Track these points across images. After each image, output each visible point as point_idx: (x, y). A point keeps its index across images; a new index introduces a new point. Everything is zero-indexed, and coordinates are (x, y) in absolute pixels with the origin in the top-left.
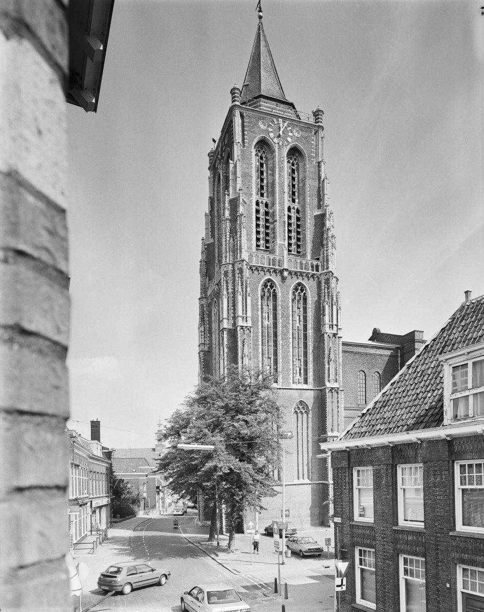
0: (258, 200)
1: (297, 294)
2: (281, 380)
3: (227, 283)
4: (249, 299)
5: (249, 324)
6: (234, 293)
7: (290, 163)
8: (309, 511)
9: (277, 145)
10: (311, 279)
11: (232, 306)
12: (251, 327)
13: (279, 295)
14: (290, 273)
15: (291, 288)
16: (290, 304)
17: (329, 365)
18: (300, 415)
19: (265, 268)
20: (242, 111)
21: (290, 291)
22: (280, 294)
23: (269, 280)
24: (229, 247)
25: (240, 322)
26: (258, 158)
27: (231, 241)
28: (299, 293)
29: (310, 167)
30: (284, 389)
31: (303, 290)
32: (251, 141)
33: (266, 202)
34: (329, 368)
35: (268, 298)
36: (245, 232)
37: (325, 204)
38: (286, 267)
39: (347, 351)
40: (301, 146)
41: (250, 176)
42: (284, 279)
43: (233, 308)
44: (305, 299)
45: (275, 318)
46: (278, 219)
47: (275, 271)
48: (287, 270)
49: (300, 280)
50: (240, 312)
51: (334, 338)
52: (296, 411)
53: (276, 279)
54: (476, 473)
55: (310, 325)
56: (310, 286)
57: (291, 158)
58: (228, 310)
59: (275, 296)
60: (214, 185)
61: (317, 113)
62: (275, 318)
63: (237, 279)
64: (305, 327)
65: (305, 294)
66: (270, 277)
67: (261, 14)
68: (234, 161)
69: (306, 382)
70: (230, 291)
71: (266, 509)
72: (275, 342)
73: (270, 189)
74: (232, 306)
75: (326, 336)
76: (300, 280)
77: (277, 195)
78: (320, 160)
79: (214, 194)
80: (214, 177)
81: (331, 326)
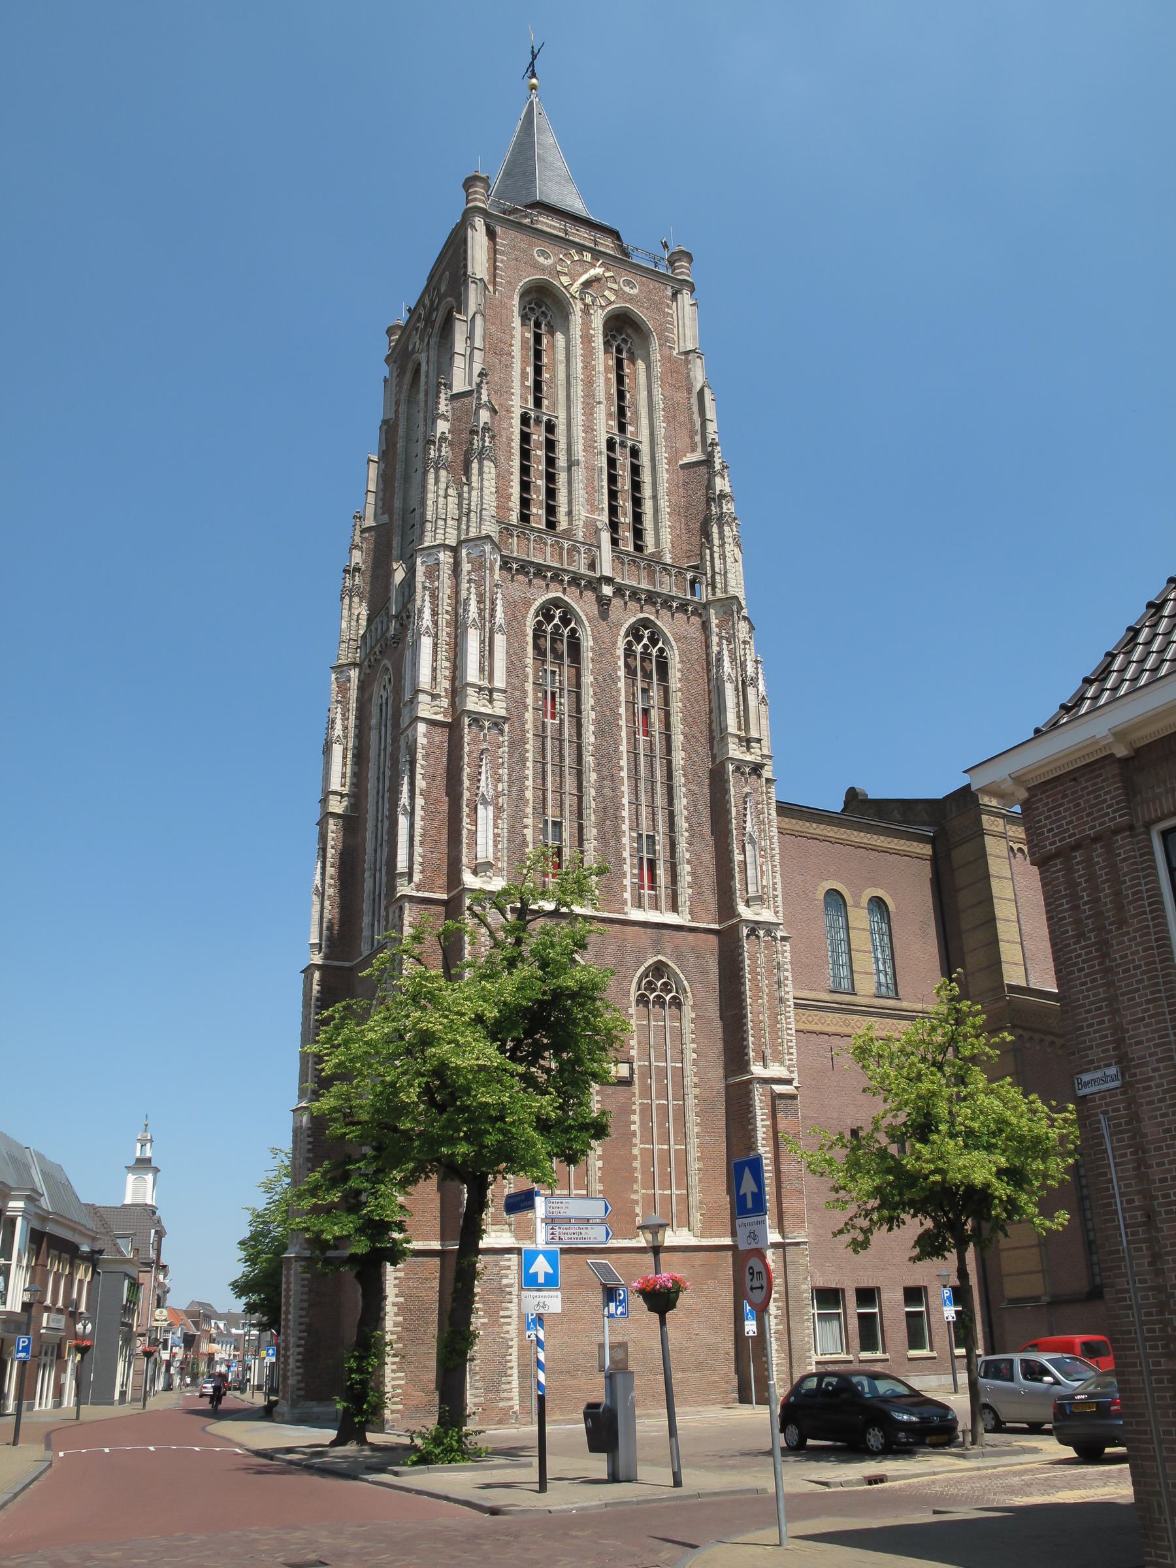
0: (526, 413)
3: (435, 598)
4: (500, 640)
5: (499, 708)
12: (506, 719)
13: (587, 643)
14: (619, 591)
15: (623, 632)
21: (620, 638)
22: (591, 643)
23: (556, 603)
28: (646, 647)
32: (511, 285)
36: (493, 470)
38: (607, 571)
40: (642, 314)
41: (509, 354)
42: (603, 604)
44: (663, 667)
47: (575, 580)
48: (609, 580)
49: (648, 613)
50: (472, 674)
53: (583, 606)
57: (613, 337)
58: (434, 670)
60: (397, 403)
63: (465, 586)
67: (534, 81)
68: (466, 314)
69: (675, 908)
71: (835, 1235)
76: (648, 613)
79: (396, 412)
80: (401, 375)
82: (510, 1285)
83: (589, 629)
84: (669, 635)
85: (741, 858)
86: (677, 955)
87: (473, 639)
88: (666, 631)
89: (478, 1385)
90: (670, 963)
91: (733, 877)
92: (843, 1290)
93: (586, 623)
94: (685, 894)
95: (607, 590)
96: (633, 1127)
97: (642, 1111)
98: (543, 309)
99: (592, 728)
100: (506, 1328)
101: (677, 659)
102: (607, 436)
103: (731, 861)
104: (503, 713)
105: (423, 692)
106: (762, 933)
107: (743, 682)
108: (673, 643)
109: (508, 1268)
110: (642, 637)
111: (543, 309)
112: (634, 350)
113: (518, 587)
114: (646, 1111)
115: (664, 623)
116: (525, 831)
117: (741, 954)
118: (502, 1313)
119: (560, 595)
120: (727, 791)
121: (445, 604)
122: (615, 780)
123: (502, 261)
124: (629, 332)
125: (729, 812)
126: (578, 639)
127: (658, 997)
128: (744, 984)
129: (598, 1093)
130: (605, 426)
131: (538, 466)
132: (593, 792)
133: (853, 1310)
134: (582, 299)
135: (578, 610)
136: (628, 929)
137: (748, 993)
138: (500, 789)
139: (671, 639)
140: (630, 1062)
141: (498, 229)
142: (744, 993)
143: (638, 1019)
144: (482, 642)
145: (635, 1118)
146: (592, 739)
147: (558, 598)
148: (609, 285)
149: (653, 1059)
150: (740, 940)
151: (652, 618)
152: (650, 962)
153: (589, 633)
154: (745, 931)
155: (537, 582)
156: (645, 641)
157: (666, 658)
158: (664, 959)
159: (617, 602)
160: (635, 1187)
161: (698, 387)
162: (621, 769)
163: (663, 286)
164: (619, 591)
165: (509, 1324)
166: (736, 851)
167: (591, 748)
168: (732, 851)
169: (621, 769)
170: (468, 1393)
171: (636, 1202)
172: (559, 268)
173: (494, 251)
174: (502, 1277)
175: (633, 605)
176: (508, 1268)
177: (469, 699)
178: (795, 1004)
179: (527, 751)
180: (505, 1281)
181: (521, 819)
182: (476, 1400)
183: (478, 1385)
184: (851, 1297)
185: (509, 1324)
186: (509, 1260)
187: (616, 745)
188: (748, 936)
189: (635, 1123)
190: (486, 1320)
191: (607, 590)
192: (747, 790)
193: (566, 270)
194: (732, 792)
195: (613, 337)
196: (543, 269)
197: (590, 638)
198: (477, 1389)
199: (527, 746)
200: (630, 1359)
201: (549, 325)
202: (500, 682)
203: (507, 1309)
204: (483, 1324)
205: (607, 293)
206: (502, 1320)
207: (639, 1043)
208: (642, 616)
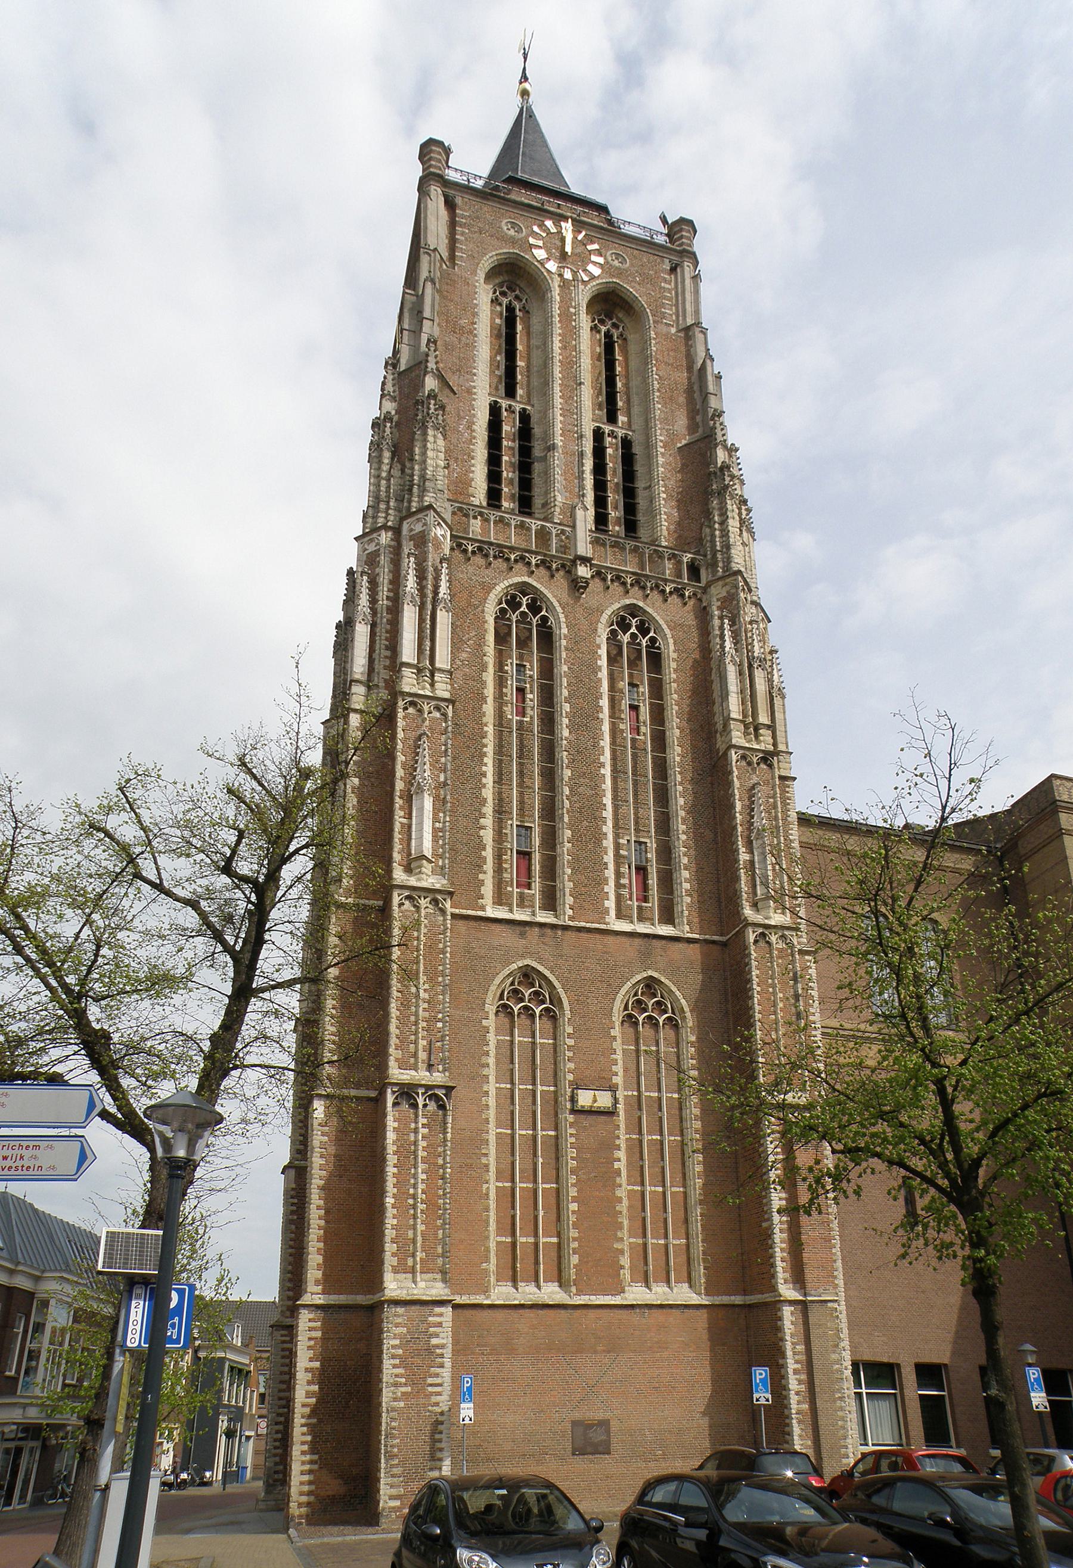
1: (626, 638)
2: (569, 900)
4: (444, 618)
6: (395, 610)
7: (599, 332)
8: (705, 1422)
9: (557, 279)
10: (674, 599)
19: (512, 549)
20: (451, 192)
22: (564, 631)
23: (524, 589)
24: (388, 487)
25: (409, 682)
26: (498, 308)
27: (396, 472)
29: (659, 336)
31: (648, 631)
33: (524, 410)
34: (752, 862)
38: (583, 547)
40: (633, 289)
42: (577, 586)
43: (388, 653)
44: (656, 660)
45: (548, 696)
46: (559, 441)
48: (585, 560)
49: (634, 598)
50: (408, 652)
52: (630, 1016)
53: (553, 592)
54: (497, 1180)
56: (669, 618)
59: (547, 637)
61: (676, 229)
62: (548, 696)
64: (660, 740)
65: (653, 640)
69: (668, 916)
70: (383, 602)
72: (550, 777)
73: (535, 382)
74: (387, 648)
75: (734, 756)
76: (634, 598)
81: (754, 728)
82: (443, 1346)
83: (561, 616)
84: (661, 622)
85: (747, 857)
86: (673, 971)
87: (409, 616)
88: (658, 618)
89: (395, 1471)
90: (663, 979)
91: (737, 879)
92: (898, 1365)
93: (559, 609)
95: (583, 571)
96: (616, 1165)
98: (517, 292)
100: (434, 1399)
103: (737, 861)
104: (446, 695)
106: (773, 939)
108: (667, 631)
109: (440, 1325)
110: (629, 627)
111: (517, 292)
112: (626, 334)
113: (474, 569)
114: (636, 1148)
116: (482, 833)
118: (430, 1381)
119: (526, 579)
120: (730, 784)
121: (384, 591)
123: (463, 234)
124: (620, 315)
125: (733, 806)
126: (550, 628)
127: (650, 1017)
128: (752, 997)
129: (572, 1125)
133: (913, 1391)
135: (549, 596)
137: (757, 1008)
138: (442, 779)
139: (664, 626)
140: (613, 1089)
141: (459, 201)
142: (752, 1008)
144: (421, 620)
145: (622, 1154)
146: (566, 733)
147: (525, 583)
150: (746, 947)
151: (641, 604)
152: (639, 977)
153: (563, 619)
154: (752, 938)
155: (499, 564)
156: (633, 630)
158: (656, 975)
159: (596, 585)
160: (619, 1235)
164: (599, 574)
165: (439, 1394)
166: (742, 850)
169: (603, 765)
170: (382, 1481)
171: (622, 1252)
173: (453, 224)
174: (432, 1336)
176: (440, 1325)
177: (405, 680)
178: (823, 1034)
180: (434, 1341)
182: (394, 1492)
183: (395, 1471)
184: (909, 1376)
185: (439, 1394)
186: (441, 1315)
187: (597, 737)
188: (756, 942)
190: (409, 1389)
191: (583, 571)
192: (755, 779)
193: (540, 243)
195: (602, 322)
196: (513, 241)
197: (563, 625)
198: (393, 1476)
200: (614, 1440)
202: (443, 659)
203: (437, 1375)
204: (404, 1394)
206: (430, 1389)
208: (628, 602)
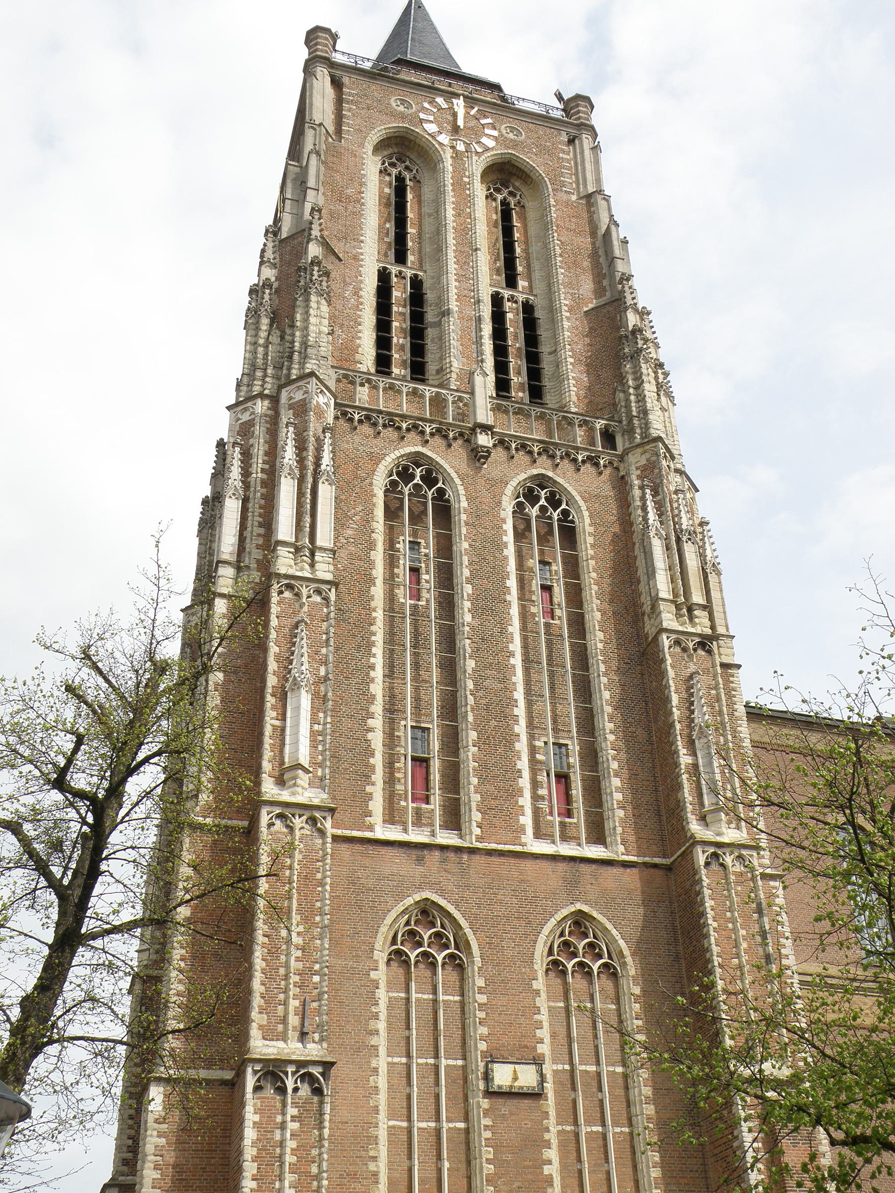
0: (385, 269)
1: (534, 512)
2: (477, 816)
4: (326, 493)
7: (495, 200)
10: (588, 468)
11: (260, 525)
13: (461, 504)
15: (509, 490)
16: (510, 551)
17: (694, 754)
18: (576, 982)
19: (404, 417)
22: (464, 504)
23: (417, 459)
28: (543, 509)
29: (559, 203)
30: (490, 853)
33: (416, 276)
35: (417, 518)
37: (618, 276)
39: (635, 1153)
40: (531, 160)
42: (478, 456)
43: (262, 531)
44: (569, 534)
46: (454, 305)
48: (485, 428)
49: (543, 468)
50: (285, 529)
51: (701, 652)
53: (451, 462)
55: (595, 613)
64: (578, 625)
65: (566, 513)
66: (424, 450)
69: (598, 835)
70: (257, 475)
72: (450, 669)
73: (428, 248)
74: (260, 525)
75: (666, 641)
76: (543, 468)
77: (451, 254)
78: (591, 189)
84: (574, 493)
86: (607, 903)
87: (287, 490)
88: (570, 489)
90: (595, 914)
91: (680, 786)
93: (458, 481)
94: (618, 816)
95: (484, 440)
96: (547, 1170)
97: (562, 1146)
98: (407, 163)
99: (467, 604)
101: (587, 521)
102: (491, 290)
103: (677, 765)
105: (225, 562)
106: (729, 860)
107: (678, 540)
111: (407, 163)
115: (565, 478)
116: (370, 736)
117: (699, 893)
119: (420, 449)
120: (663, 674)
122: (504, 673)
124: (517, 184)
125: (668, 700)
126: (448, 501)
128: (707, 936)
129: (486, 1113)
130: (487, 280)
131: (399, 324)
132: (470, 685)
134: (453, 147)
136: (528, 864)
137: (715, 949)
138: (322, 672)
139: (578, 498)
140: (538, 1061)
141: (346, 80)
142: (708, 950)
143: (549, 999)
144: (300, 494)
145: (552, 1154)
146: (468, 618)
148: (487, 131)
149: (577, 1060)
150: (695, 872)
152: (565, 912)
154: (701, 859)
156: (543, 502)
157: (572, 522)
158: (586, 908)
159: (499, 454)
161: (604, 228)
162: (512, 654)
163: (556, 133)
164: (502, 443)
166: (683, 751)
167: (467, 629)
168: (676, 752)
169: (512, 654)
172: (422, 116)
173: (339, 102)
175: (521, 457)
177: (281, 561)
178: (801, 982)
179: (374, 634)
181: (364, 720)
188: (707, 864)
189: (549, 1162)
191: (484, 440)
192: (692, 668)
193: (431, 118)
194: (671, 673)
195: (498, 190)
196: (403, 117)
199: (373, 628)
201: (414, 179)
202: (325, 537)
205: (484, 140)
207: (553, 1035)
208: (535, 472)
